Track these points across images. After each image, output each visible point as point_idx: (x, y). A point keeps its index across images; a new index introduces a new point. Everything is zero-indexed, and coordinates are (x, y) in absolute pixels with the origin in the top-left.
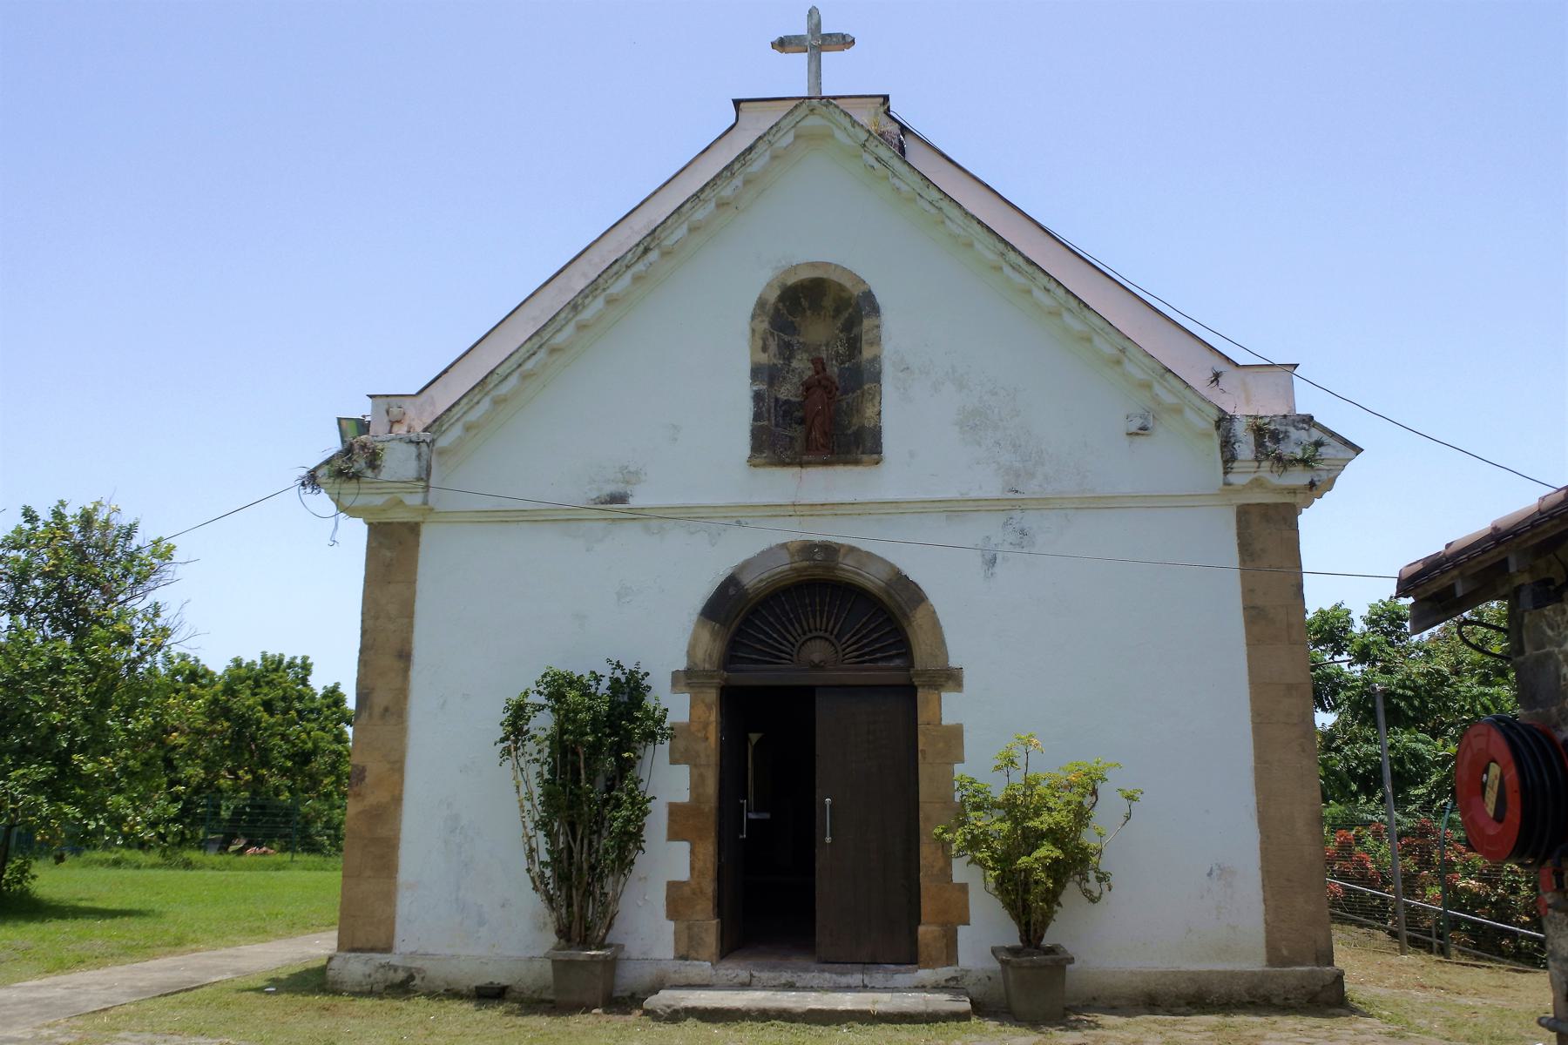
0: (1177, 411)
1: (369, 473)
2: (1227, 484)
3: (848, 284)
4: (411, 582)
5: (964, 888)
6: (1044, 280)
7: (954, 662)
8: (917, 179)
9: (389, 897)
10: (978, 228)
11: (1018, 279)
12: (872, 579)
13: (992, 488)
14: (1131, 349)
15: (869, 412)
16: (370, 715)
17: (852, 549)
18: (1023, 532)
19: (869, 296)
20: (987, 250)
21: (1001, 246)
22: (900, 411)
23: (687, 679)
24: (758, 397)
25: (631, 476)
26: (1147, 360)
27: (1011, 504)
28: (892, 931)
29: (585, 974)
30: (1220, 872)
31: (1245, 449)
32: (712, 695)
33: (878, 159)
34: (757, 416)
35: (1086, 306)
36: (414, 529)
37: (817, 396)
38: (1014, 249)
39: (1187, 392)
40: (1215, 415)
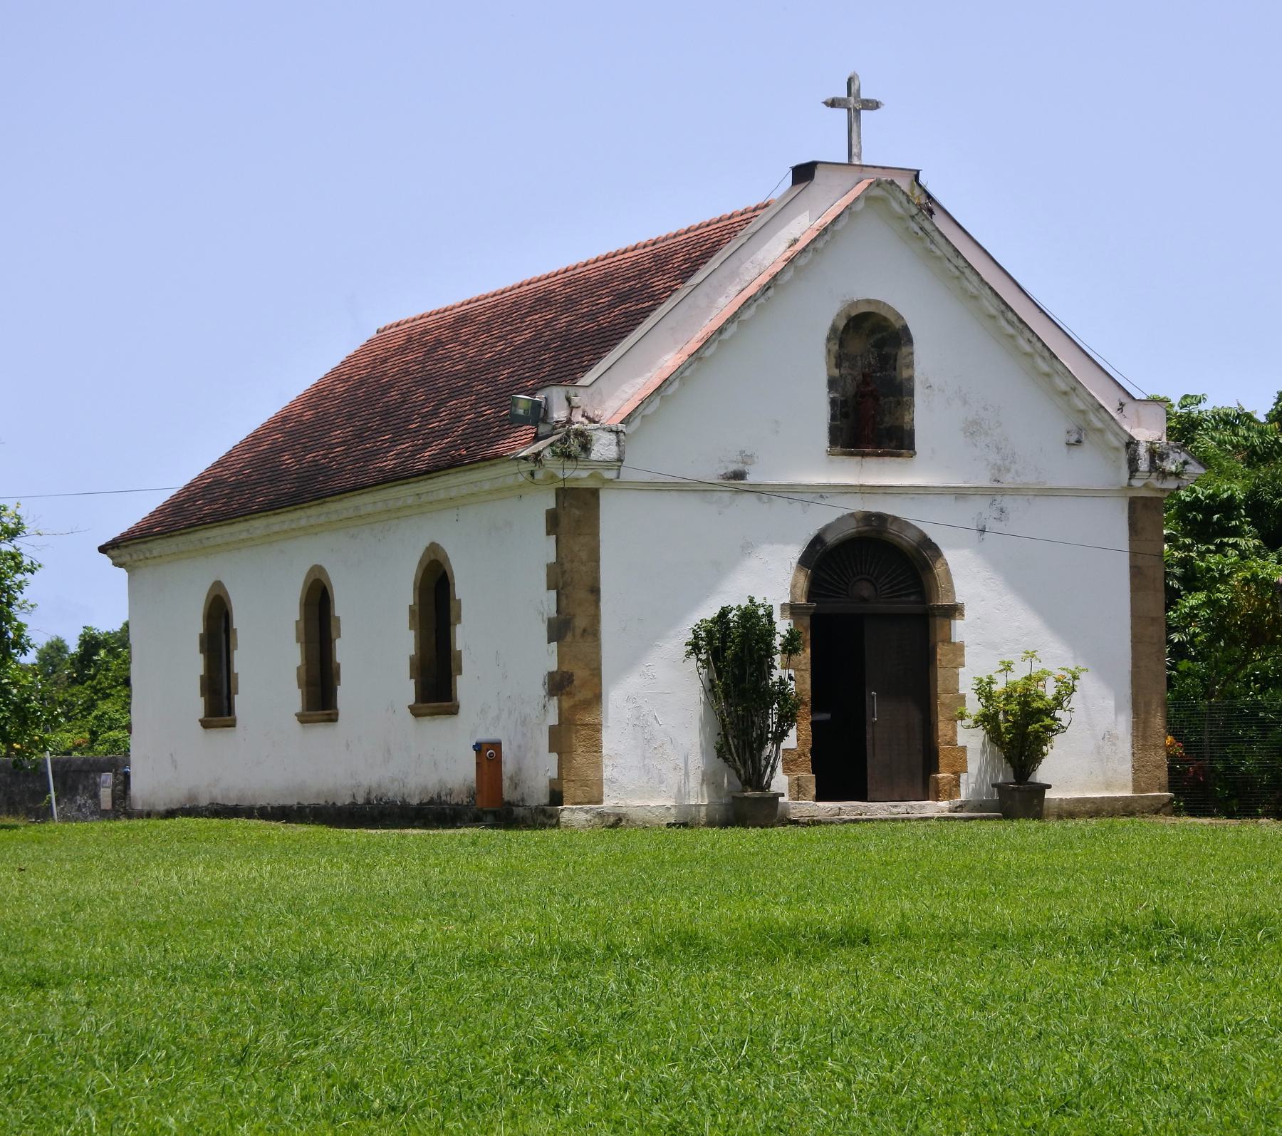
0: (1100, 431)
1: (583, 455)
2: (1130, 485)
3: (893, 319)
4: (595, 535)
5: (964, 749)
6: (1029, 335)
7: (959, 599)
8: (951, 250)
9: (598, 766)
10: (989, 292)
11: (1010, 330)
12: (909, 538)
13: (983, 480)
14: (1081, 389)
15: (907, 419)
16: (574, 635)
17: (896, 519)
18: (1002, 511)
19: (905, 329)
20: (991, 306)
21: (1003, 307)
22: (928, 416)
23: (793, 610)
24: (833, 402)
25: (747, 458)
26: (1088, 398)
27: (993, 493)
28: (922, 769)
29: (747, 807)
30: (1109, 736)
31: (1144, 465)
32: (807, 621)
33: (921, 229)
34: (833, 418)
35: (1055, 357)
36: (594, 493)
37: (870, 407)
38: (1012, 310)
39: (1112, 423)
40: (1127, 439)
